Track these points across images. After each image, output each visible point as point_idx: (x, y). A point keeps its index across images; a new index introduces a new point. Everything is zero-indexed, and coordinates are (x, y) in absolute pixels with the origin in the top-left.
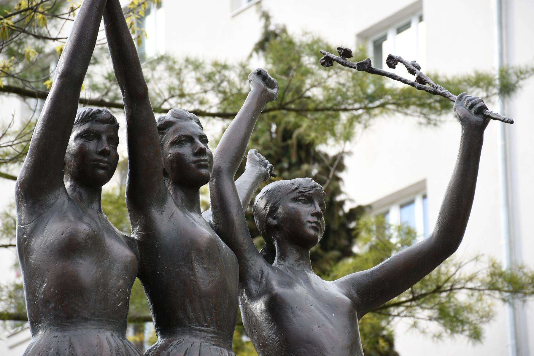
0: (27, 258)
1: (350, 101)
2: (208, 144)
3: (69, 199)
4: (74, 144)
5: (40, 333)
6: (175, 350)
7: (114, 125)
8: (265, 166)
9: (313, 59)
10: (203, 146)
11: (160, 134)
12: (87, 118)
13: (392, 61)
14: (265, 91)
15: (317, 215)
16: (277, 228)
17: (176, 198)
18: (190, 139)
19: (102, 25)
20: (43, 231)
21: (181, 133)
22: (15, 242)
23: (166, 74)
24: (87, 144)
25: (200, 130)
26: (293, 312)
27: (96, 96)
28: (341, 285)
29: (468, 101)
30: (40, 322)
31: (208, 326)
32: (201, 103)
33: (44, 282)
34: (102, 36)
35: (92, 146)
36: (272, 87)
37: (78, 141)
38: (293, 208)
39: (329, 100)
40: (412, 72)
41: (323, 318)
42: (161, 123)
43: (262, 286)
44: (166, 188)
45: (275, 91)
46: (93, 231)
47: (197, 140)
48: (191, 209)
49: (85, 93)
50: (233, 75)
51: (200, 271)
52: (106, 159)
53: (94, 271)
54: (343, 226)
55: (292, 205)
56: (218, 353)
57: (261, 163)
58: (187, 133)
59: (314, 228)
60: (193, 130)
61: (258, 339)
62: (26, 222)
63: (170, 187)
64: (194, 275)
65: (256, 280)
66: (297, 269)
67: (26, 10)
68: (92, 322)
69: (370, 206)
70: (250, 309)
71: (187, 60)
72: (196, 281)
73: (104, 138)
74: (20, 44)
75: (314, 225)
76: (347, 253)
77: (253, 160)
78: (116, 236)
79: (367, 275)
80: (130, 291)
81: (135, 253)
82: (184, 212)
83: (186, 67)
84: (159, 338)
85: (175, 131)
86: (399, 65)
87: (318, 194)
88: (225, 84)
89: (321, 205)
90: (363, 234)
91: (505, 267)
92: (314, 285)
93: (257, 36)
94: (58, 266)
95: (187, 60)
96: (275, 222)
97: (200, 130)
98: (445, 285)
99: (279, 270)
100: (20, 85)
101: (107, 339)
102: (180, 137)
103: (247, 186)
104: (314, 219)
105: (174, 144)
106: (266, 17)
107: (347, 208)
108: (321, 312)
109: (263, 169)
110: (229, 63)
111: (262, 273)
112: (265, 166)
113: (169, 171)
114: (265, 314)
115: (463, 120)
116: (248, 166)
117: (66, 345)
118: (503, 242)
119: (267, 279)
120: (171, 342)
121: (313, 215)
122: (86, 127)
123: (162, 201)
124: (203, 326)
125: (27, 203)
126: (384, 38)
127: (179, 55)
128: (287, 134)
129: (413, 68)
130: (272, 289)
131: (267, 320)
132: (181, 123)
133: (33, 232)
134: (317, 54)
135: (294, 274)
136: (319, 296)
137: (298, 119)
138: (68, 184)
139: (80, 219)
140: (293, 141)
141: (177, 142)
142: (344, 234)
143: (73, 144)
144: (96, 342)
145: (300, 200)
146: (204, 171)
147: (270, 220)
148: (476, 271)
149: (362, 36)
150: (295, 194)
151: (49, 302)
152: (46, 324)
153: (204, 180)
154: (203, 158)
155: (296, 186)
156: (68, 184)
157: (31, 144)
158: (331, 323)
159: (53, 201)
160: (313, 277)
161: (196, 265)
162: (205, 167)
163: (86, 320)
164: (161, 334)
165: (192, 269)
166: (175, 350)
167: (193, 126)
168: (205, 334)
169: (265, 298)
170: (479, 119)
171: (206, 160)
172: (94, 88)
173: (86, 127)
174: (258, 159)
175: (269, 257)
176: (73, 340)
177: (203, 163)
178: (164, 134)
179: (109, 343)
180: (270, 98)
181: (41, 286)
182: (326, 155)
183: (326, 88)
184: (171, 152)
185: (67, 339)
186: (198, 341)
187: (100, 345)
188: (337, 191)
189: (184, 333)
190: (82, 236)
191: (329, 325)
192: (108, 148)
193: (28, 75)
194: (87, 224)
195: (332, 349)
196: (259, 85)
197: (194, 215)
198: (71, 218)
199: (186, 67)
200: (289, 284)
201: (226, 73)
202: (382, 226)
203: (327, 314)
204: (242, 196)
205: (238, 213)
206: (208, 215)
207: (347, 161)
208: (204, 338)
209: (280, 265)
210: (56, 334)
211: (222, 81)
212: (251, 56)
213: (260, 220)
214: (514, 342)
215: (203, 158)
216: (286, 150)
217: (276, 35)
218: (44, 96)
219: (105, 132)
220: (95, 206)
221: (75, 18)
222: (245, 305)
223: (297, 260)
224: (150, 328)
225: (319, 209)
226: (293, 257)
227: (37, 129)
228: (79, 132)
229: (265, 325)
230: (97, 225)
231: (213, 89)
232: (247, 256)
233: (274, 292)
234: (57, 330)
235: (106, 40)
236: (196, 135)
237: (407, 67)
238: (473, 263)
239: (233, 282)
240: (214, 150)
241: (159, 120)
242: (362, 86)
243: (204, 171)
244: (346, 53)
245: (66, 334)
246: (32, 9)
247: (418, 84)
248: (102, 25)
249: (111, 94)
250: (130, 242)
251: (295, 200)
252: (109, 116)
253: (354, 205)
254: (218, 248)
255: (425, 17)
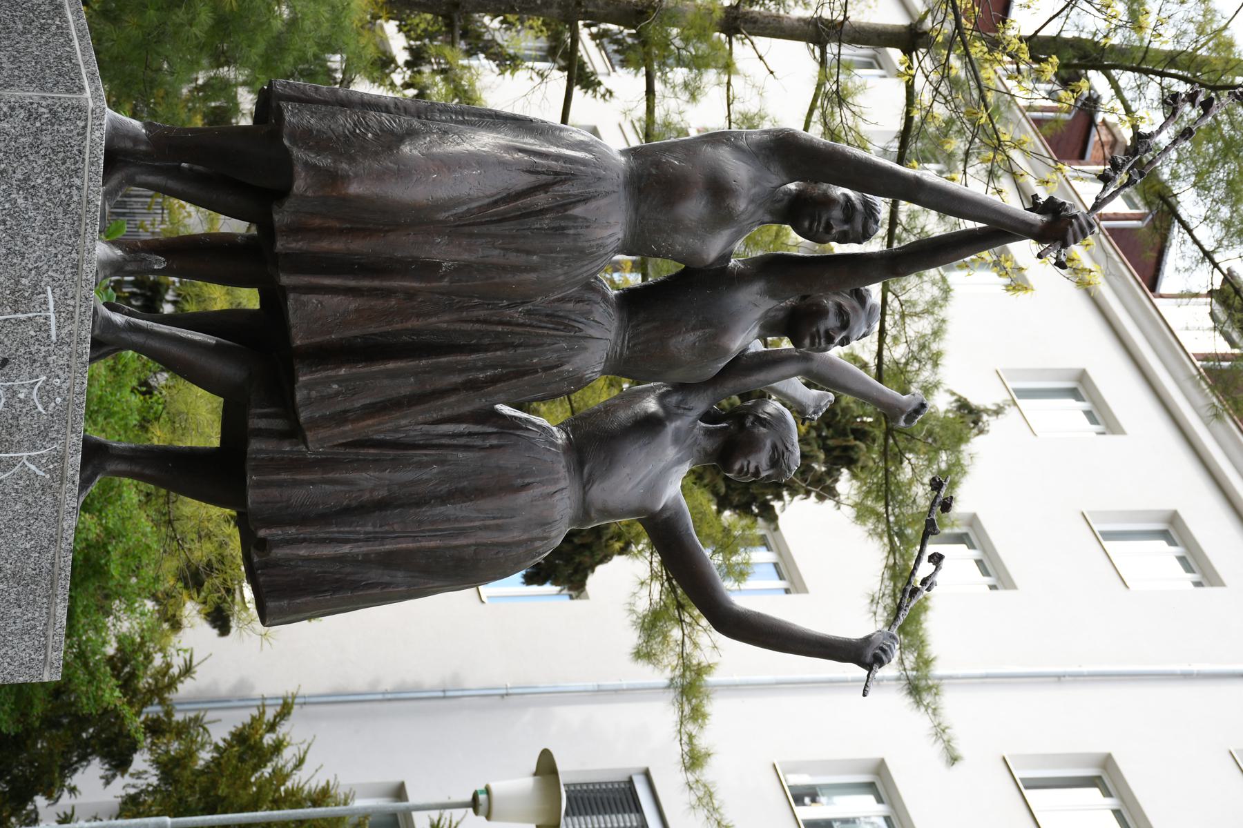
0: (707, 142)
1: (897, 510)
2: (839, 347)
3: (776, 188)
4: (839, 193)
5: (623, 159)
6: (601, 310)
7: (864, 236)
8: (815, 413)
9: (943, 466)
10: (837, 341)
11: (851, 291)
12: (870, 211)
13: (937, 559)
14: (902, 412)
15: (757, 472)
16: (742, 426)
17: (777, 310)
18: (845, 325)
19: (980, 225)
20: (738, 159)
21: (851, 315)
22: (734, 128)
23: (928, 297)
24: (839, 208)
25: (855, 337)
26: (645, 445)
27: (903, 217)
28: (676, 500)
29: (889, 646)
30: (634, 158)
31: (628, 347)
32: (895, 339)
33: (680, 161)
34: (970, 225)
35: (837, 213)
36: (906, 421)
37: (842, 198)
38: (765, 445)
39: (898, 484)
40: (924, 582)
41: (638, 480)
42: (864, 292)
43: (675, 409)
44: (788, 298)
45: (902, 424)
46: (738, 216)
47: (843, 334)
48: (763, 327)
49: (905, 207)
50: (926, 374)
51: (691, 337)
52: (821, 230)
53: (692, 218)
54: (754, 499)
55: (768, 443)
56: (598, 359)
57: (818, 408)
58: (852, 323)
59: (742, 468)
60: (856, 329)
61: (614, 405)
62: (749, 140)
63: (789, 302)
64: (687, 331)
65: (681, 401)
66: (695, 450)
67: (998, 138)
68: (634, 217)
69: (776, 528)
70: (649, 396)
71: (943, 321)
72: (680, 333)
73: (846, 227)
74: (961, 132)
75: (745, 469)
76: (723, 504)
77: (821, 398)
78: (732, 241)
79: (688, 529)
80: (668, 258)
81: (712, 264)
82: (760, 319)
83: (936, 320)
84: (616, 292)
85: (853, 308)
86: (932, 567)
87: (782, 473)
88: (916, 365)
89: (768, 477)
90: (746, 521)
91: (710, 679)
92: (676, 468)
93: (975, 400)
94: (698, 176)
95: (943, 321)
96: (748, 424)
97: (855, 337)
98: (686, 614)
99: (693, 428)
100: (914, 131)
101: (615, 234)
102: (848, 314)
103: (790, 391)
104: (752, 469)
105: (839, 307)
106: (998, 411)
107: (777, 505)
108: (645, 477)
109: (811, 410)
110: (941, 369)
111: (690, 410)
112: (815, 413)
113: (808, 301)
114: (642, 413)
115: (867, 640)
116: (815, 392)
117: (609, 188)
118: (737, 678)
119: (683, 415)
120: (611, 305)
121: (757, 468)
122: (859, 206)
123: (772, 293)
124: (629, 342)
125: (771, 141)
126: (971, 546)
127: (949, 311)
128: (861, 434)
129: (929, 583)
130: (671, 421)
131: (636, 415)
132: (863, 316)
133: (737, 148)
134: (949, 470)
135: (689, 446)
136: (664, 474)
137: (140, 737)
138: (792, 186)
139: (752, 201)
140: (852, 442)
141: (841, 311)
142: (744, 500)
143: (839, 191)
144: (612, 220)
145: (773, 452)
146: (807, 342)
147: (751, 418)
148: (702, 647)
149: (973, 521)
150: (781, 447)
151: (657, 168)
152: (633, 165)
153: (796, 342)
154: (823, 341)
155: (790, 448)
156: (792, 186)
157: (842, 146)
158: (633, 488)
159: (772, 170)
160: (686, 468)
161: (698, 333)
162: (813, 344)
163: (637, 209)
164: (621, 294)
165: (694, 329)
166: (601, 310)
167: (860, 330)
168: (620, 344)
169: (661, 412)
170: (869, 658)
171: (820, 344)
172: (912, 216)
173: (859, 206)
174: (822, 404)
175: (707, 417)
176: (614, 196)
177: (817, 340)
178: (851, 296)
179: (610, 236)
180: (895, 418)
181: (676, 158)
182: (836, 480)
183: (910, 483)
184: (829, 303)
185: (616, 189)
186: (612, 336)
187: (608, 225)
188: (794, 493)
189: (621, 320)
190: (732, 203)
191: (629, 487)
192: (834, 231)
193: (926, 141)
194: (746, 209)
195: (603, 489)
196: (909, 405)
197: (756, 331)
198: (753, 191)
199: (936, 320)
200: (677, 440)
201: (929, 367)
202: (750, 543)
203: (642, 484)
204: (779, 385)
205: (758, 381)
206: (757, 346)
207: (829, 503)
208: (616, 343)
209: (699, 429)
210: (621, 177)
211: (920, 362)
212: (953, 394)
213: (751, 406)
214: (625, 687)
215: (823, 341)
216: (843, 433)
217: (976, 423)
218: (901, 160)
219: (853, 228)
220: (767, 218)
221: (989, 195)
222: (653, 390)
223: (704, 449)
224: (635, 280)
225: (764, 474)
226: (708, 445)
227: (859, 153)
228: (853, 199)
229: (630, 412)
230: (744, 220)
231: (911, 351)
232: (709, 392)
233: (668, 423)
234: (625, 177)
235: (963, 228)
236: (849, 333)
237: (930, 576)
238: (711, 644)
239: (679, 375)
240: (835, 352)
241: (867, 290)
242: (915, 521)
243: (807, 342)
244: (946, 506)
245: (621, 188)
246: (1000, 145)
247: (909, 589)
248: (980, 225)
249: (904, 235)
250: (725, 257)
251: (774, 447)
252: (871, 233)
253: (778, 511)
254: (717, 360)
255: (994, 592)
